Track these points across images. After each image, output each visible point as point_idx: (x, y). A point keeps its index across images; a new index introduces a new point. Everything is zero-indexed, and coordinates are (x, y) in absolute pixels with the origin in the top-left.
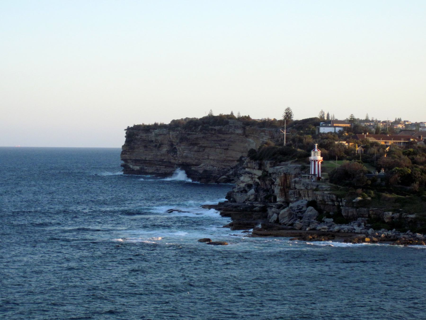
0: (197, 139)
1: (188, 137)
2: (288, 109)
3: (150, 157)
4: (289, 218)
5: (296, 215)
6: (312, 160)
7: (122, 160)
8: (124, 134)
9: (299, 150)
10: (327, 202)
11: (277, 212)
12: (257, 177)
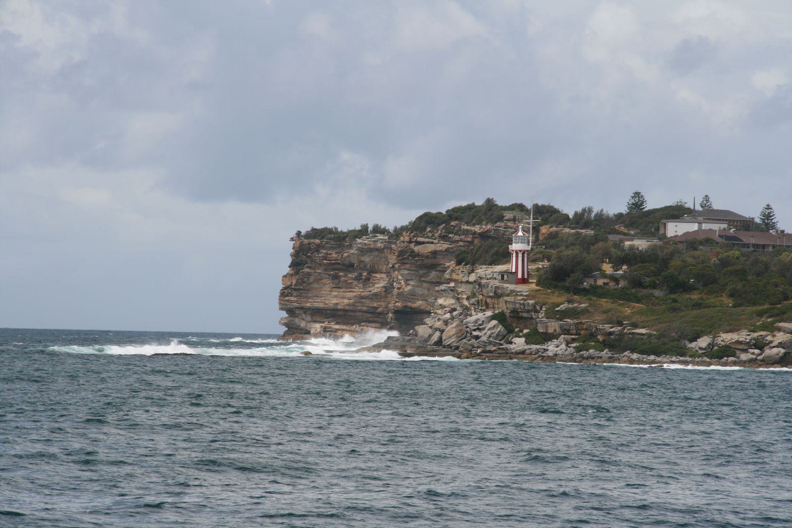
0: (435, 253)
1: (417, 249)
2: (637, 194)
3: (346, 301)
4: (458, 337)
5: (471, 334)
6: (513, 251)
7: (281, 309)
8: (288, 249)
9: (769, 320)
10: (520, 314)
11: (441, 329)
12: (465, 296)
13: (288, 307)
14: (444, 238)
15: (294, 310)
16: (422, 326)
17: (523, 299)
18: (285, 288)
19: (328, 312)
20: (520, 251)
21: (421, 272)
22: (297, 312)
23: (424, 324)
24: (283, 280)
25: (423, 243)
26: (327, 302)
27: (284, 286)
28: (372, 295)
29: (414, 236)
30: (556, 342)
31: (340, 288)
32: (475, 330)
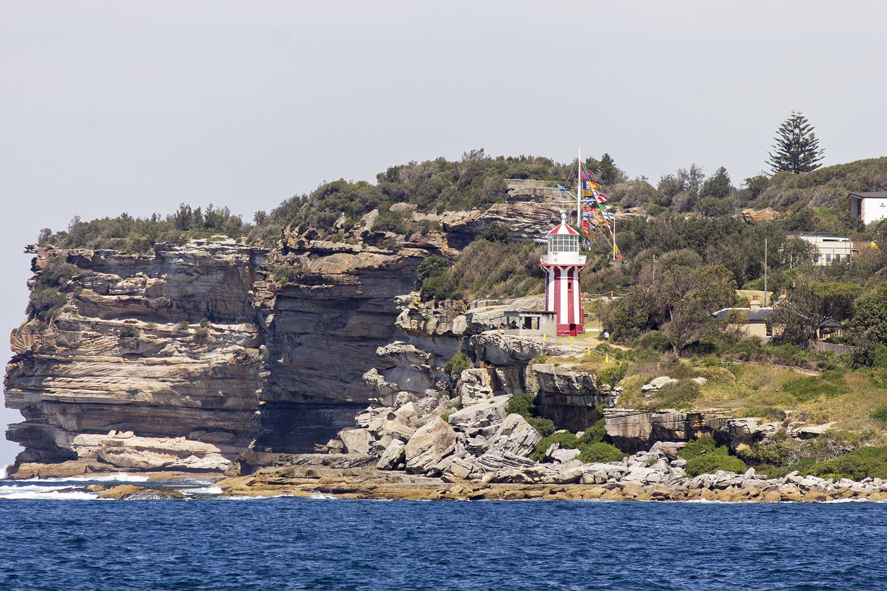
6: (548, 267)
13: (26, 400)
14: (371, 239)
15: (39, 406)
16: (352, 431)
17: (574, 369)
18: (15, 360)
19: (116, 409)
20: (564, 267)
21: (325, 316)
22: (46, 411)
23: (355, 425)
24: (12, 341)
25: (330, 252)
26: (111, 387)
27: (14, 354)
28: (214, 369)
29: (309, 238)
30: (645, 456)
31: (141, 355)
32: (473, 436)
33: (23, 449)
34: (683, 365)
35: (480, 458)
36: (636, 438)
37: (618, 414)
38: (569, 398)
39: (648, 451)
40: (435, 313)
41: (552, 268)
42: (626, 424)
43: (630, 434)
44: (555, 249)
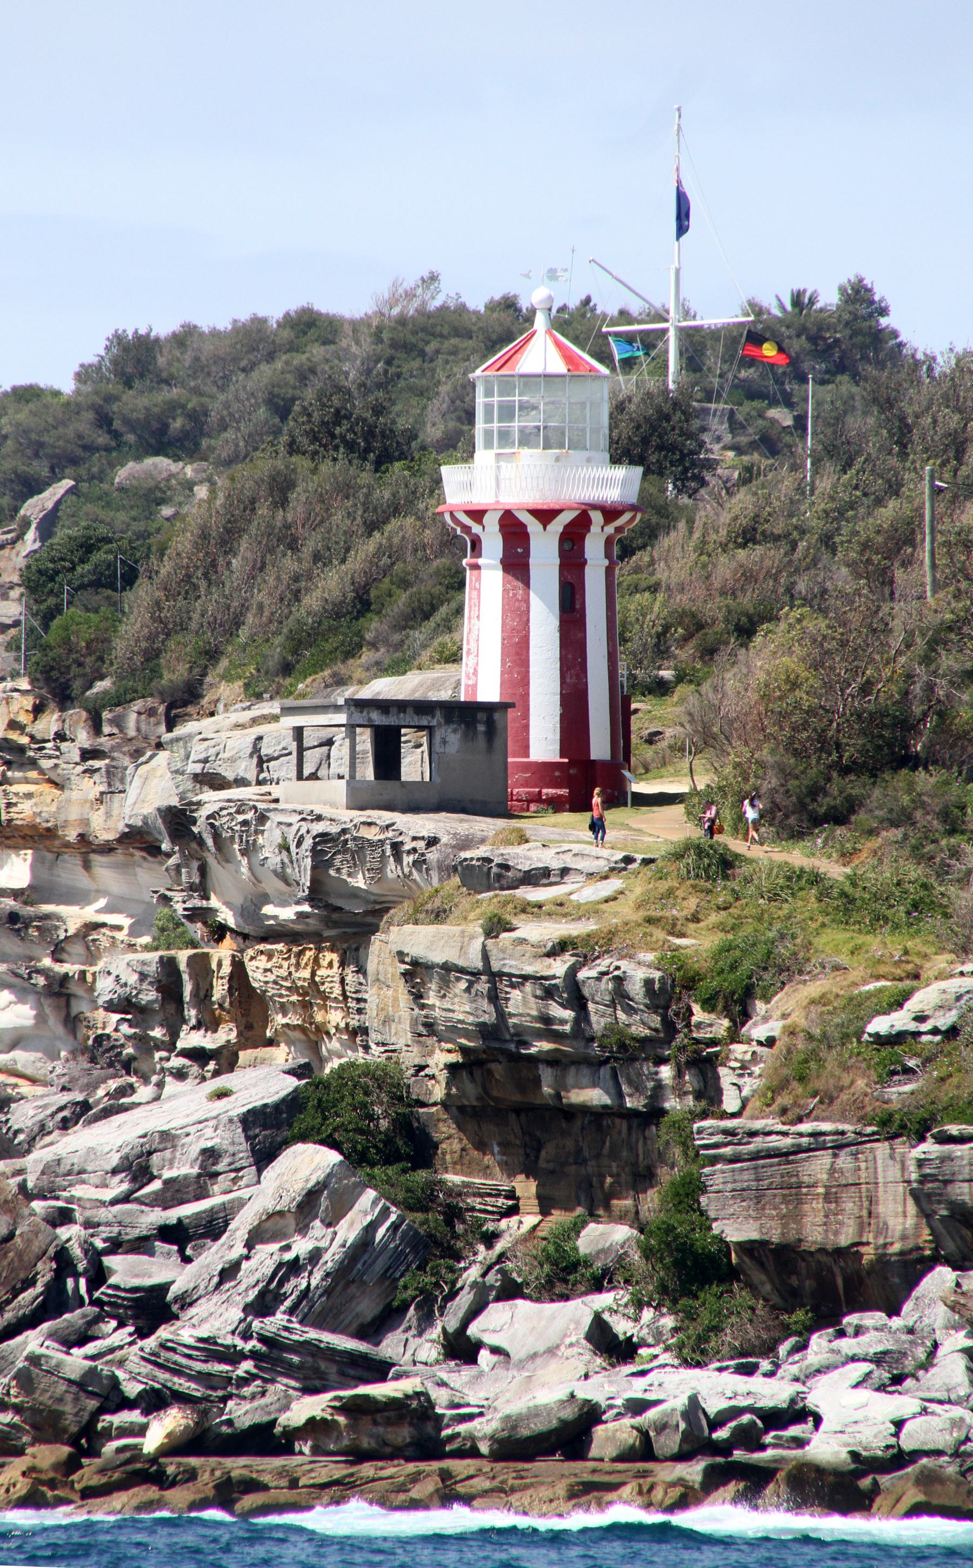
6: (477, 515)
20: (545, 516)
30: (873, 1330)
33: (334, 1157)
34: (773, 421)
35: (150, 1343)
36: (839, 1252)
37: (758, 1143)
38: (547, 1076)
39: (893, 1311)
40: (87, 755)
41: (492, 521)
42: (795, 1192)
43: (814, 1232)
44: (505, 436)
